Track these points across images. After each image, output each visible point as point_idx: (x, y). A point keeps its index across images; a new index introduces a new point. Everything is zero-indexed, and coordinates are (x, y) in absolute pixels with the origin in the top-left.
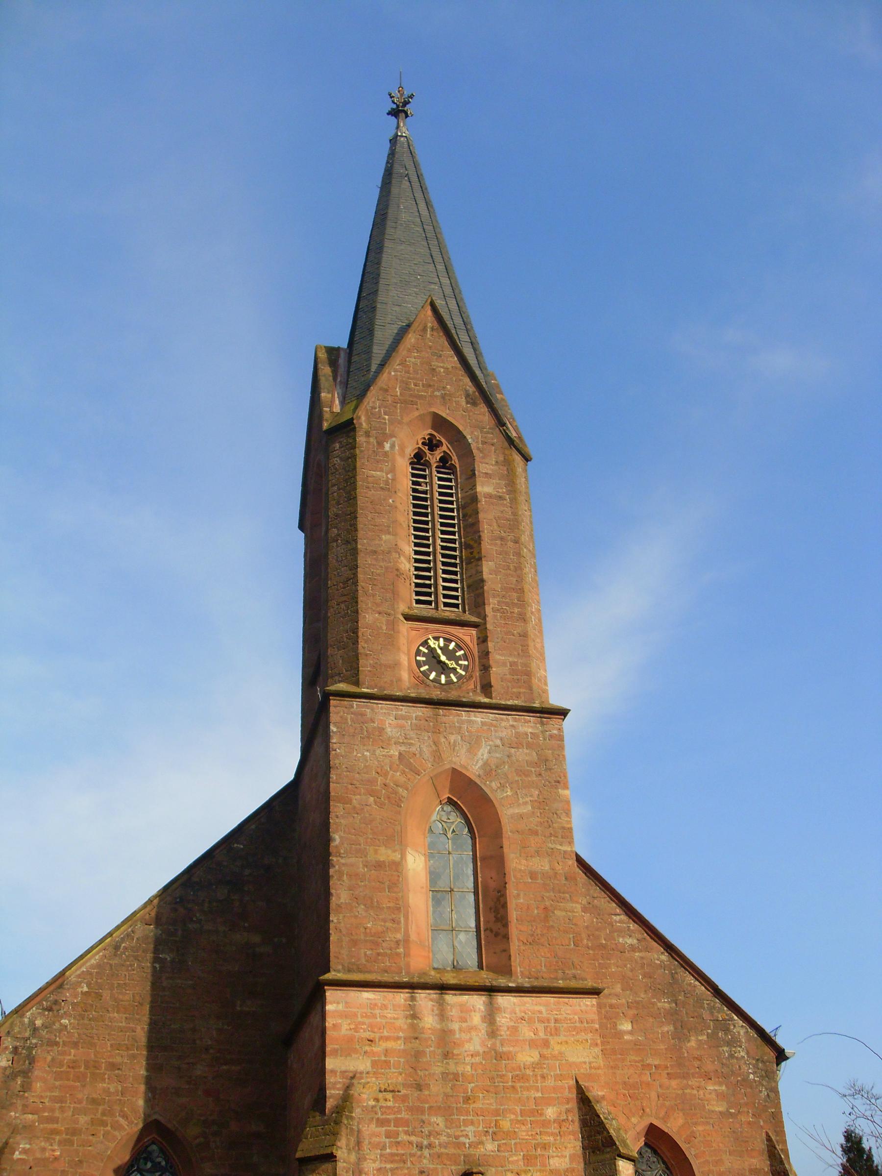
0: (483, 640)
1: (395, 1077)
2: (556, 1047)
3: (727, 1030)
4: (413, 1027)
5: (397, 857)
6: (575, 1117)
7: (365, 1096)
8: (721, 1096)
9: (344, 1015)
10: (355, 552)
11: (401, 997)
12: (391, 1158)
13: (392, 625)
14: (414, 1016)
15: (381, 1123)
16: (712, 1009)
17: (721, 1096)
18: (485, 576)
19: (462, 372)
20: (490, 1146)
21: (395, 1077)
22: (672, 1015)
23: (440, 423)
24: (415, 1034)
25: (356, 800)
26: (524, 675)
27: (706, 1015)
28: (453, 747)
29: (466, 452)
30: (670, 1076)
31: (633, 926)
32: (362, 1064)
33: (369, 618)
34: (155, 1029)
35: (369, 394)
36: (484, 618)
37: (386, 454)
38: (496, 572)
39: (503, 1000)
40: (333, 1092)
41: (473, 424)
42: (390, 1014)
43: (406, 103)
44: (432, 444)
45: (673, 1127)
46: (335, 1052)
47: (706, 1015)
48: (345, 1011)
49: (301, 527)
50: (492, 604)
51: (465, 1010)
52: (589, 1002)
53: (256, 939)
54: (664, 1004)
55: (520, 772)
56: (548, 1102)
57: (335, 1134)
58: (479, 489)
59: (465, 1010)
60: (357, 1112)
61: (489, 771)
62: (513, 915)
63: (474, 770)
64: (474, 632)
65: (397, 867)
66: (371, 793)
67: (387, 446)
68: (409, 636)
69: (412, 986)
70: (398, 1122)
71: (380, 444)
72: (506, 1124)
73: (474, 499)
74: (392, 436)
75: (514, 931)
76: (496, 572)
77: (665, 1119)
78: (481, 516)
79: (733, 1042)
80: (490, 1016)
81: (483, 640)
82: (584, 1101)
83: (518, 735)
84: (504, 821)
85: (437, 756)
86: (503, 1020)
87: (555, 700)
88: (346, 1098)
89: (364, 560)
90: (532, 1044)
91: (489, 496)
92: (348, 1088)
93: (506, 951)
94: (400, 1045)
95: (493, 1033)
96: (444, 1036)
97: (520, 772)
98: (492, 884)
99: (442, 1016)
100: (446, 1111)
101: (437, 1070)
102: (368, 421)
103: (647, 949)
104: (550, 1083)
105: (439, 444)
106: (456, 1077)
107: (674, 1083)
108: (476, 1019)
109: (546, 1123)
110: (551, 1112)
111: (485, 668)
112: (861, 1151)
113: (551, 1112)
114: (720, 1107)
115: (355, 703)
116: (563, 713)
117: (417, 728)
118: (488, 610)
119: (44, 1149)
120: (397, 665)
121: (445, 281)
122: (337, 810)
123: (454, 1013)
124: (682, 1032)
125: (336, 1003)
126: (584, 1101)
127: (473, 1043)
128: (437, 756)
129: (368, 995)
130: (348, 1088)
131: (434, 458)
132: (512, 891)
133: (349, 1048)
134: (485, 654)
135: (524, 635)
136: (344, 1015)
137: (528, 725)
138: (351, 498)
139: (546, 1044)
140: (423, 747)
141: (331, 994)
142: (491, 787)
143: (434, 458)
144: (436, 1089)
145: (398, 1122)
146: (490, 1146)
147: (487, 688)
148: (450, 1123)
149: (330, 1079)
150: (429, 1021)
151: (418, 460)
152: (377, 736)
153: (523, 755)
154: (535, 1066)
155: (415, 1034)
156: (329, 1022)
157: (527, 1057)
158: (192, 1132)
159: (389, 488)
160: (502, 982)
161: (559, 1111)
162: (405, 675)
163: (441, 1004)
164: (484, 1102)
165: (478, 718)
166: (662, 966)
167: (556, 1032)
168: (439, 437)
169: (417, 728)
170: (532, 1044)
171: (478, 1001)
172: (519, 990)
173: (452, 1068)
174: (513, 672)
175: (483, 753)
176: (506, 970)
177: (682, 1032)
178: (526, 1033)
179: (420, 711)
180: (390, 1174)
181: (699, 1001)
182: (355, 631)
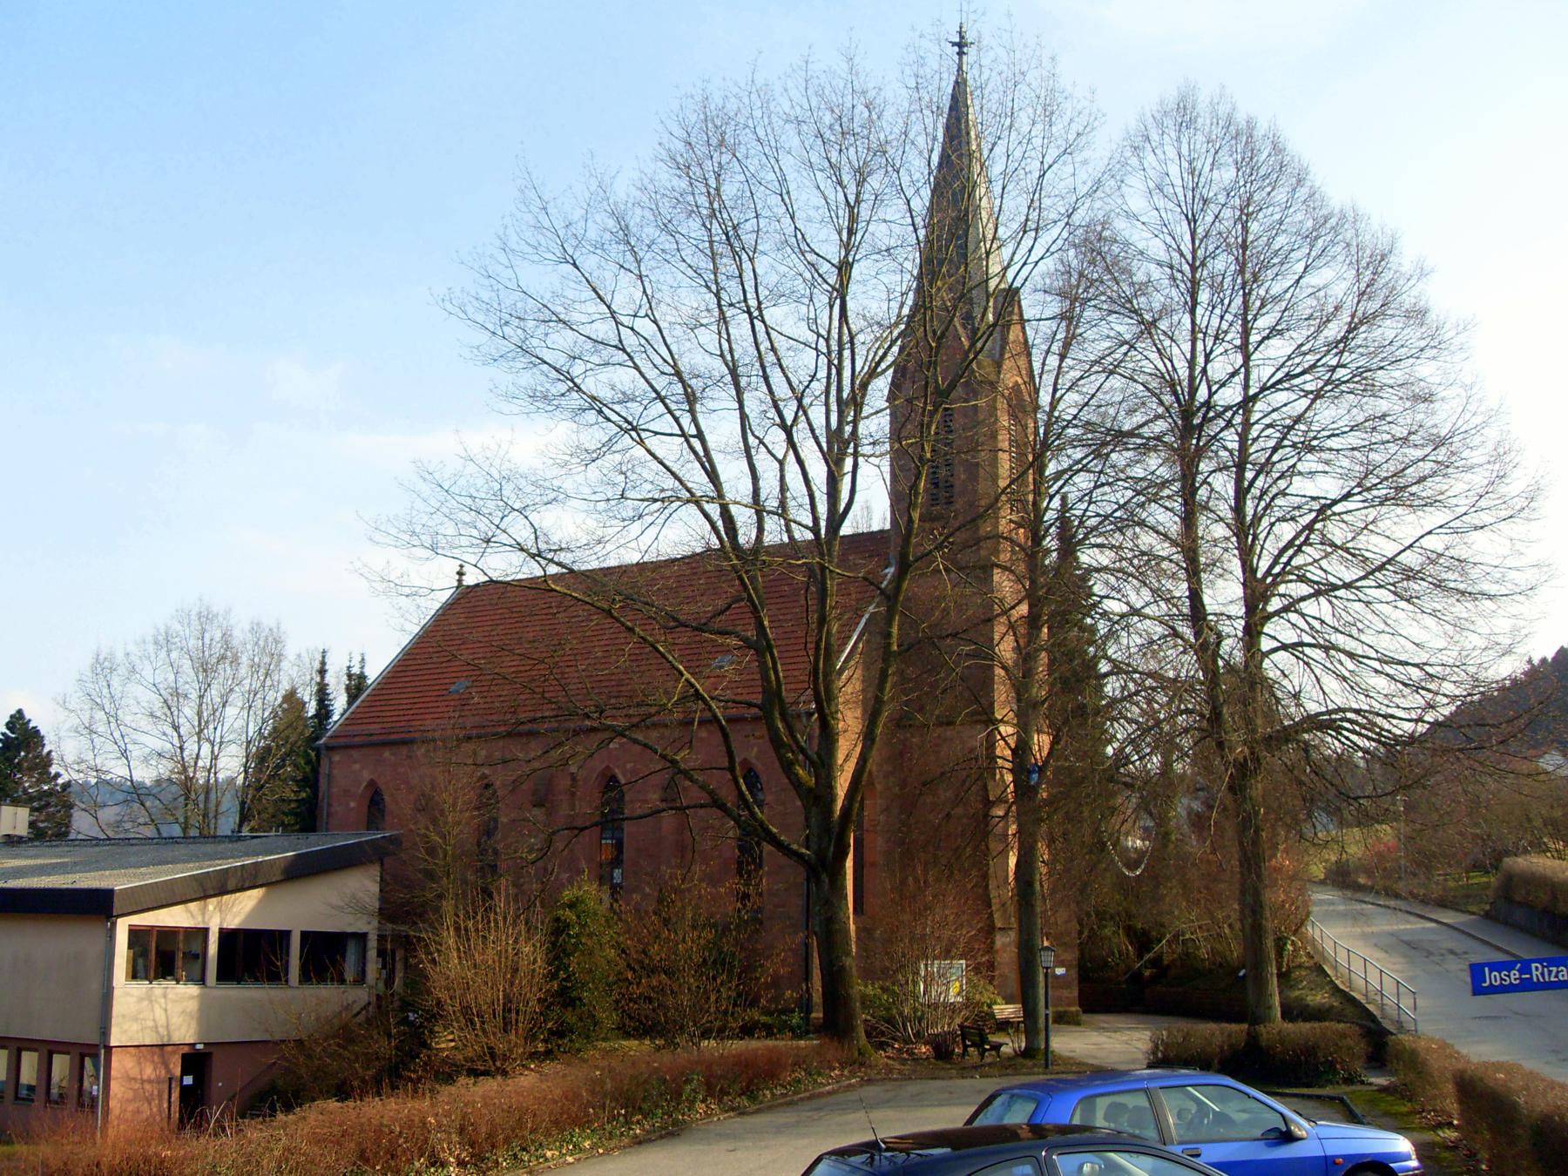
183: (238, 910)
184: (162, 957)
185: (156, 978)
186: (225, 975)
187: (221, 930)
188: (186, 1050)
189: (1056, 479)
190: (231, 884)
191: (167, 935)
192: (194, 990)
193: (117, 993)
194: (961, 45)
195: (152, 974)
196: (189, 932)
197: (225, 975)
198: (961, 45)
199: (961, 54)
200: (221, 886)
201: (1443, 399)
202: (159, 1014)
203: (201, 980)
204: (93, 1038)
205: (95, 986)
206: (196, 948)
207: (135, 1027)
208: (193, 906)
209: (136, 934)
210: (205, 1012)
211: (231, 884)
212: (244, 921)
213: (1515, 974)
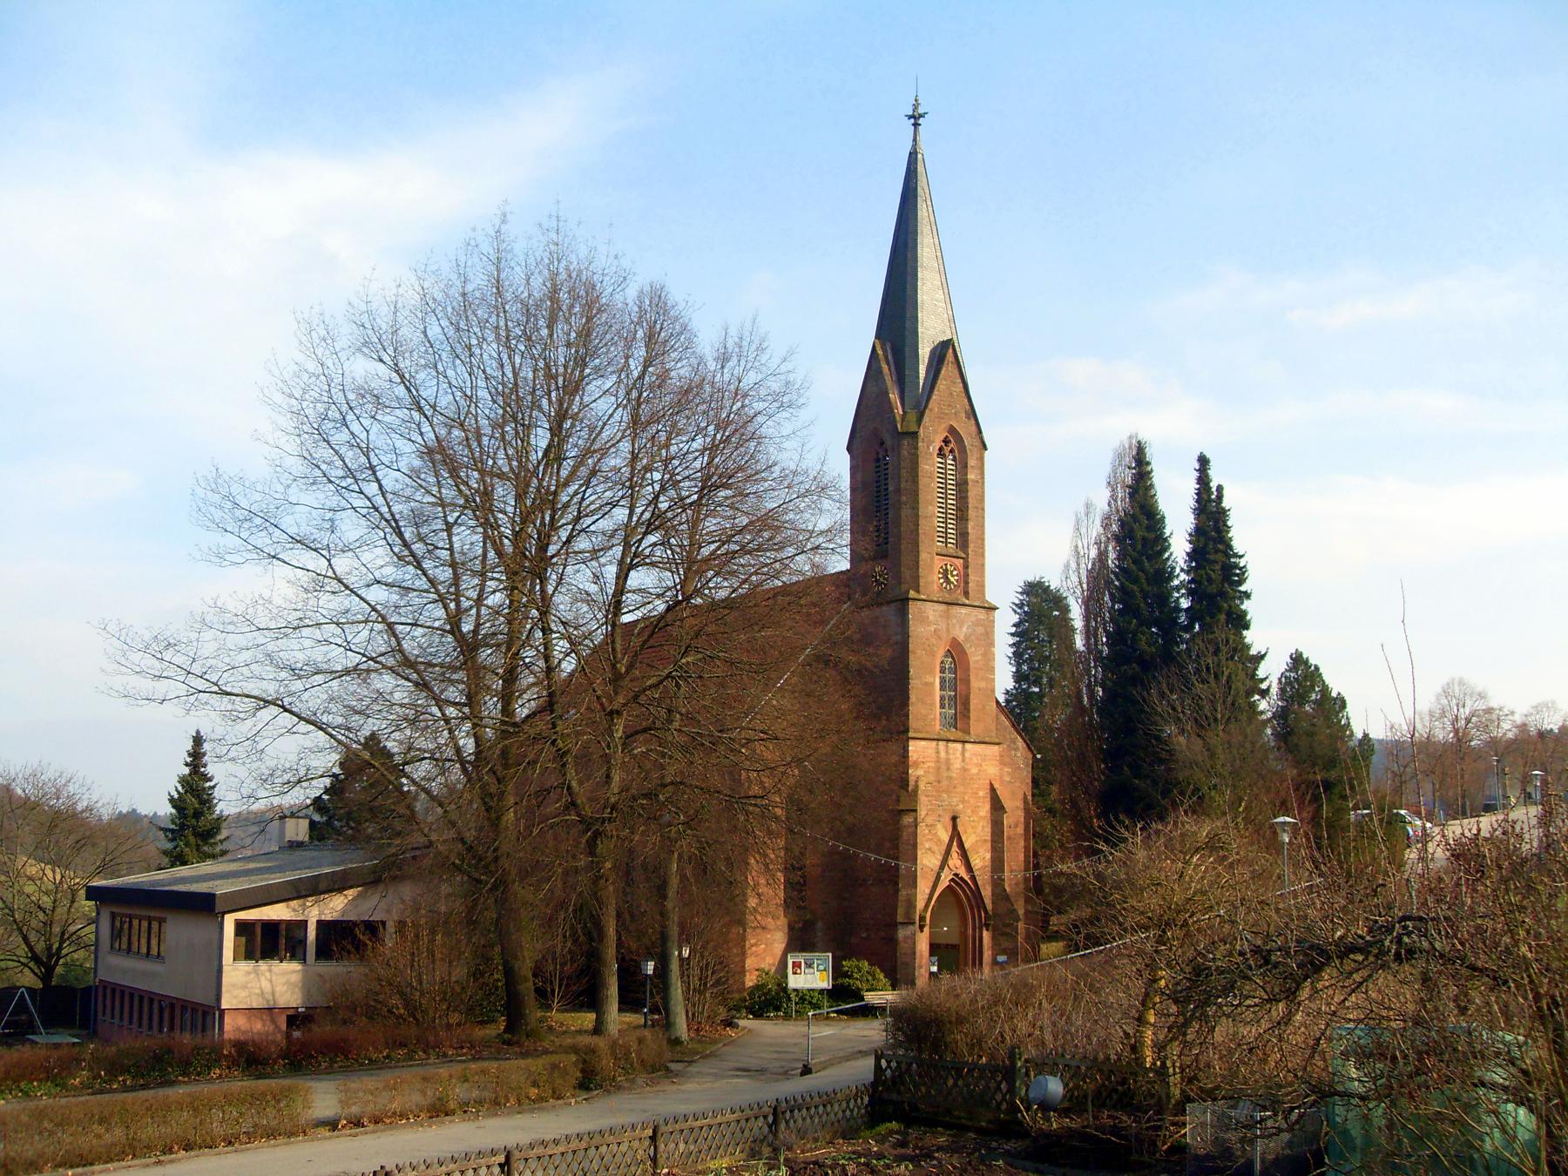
0: (966, 567)
1: (932, 778)
7: (922, 786)
21: (932, 778)
23: (952, 430)
24: (938, 761)
29: (963, 450)
40: (912, 783)
41: (965, 430)
49: (849, 449)
63: (961, 638)
68: (939, 562)
73: (966, 482)
75: (973, 715)
80: (964, 750)
81: (966, 567)
82: (993, 789)
87: (994, 603)
88: (917, 786)
96: (948, 760)
100: (947, 792)
108: (958, 754)
110: (981, 794)
111: (966, 583)
113: (981, 794)
119: (99, 1136)
126: (993, 789)
127: (957, 765)
134: (967, 575)
137: (982, 614)
141: (911, 743)
142: (966, 646)
144: (945, 783)
147: (966, 594)
150: (943, 754)
151: (941, 453)
157: (974, 771)
161: (984, 793)
164: (960, 789)
165: (964, 610)
171: (959, 746)
179: (943, 607)
180: (539, 1174)
183: (335, 906)
184: (267, 942)
185: (263, 958)
186: (323, 952)
187: (318, 922)
188: (291, 1012)
189: (593, 513)
190: (322, 886)
191: (271, 927)
192: (295, 966)
193: (225, 969)
194: (916, 118)
195: (258, 954)
196: (290, 924)
197: (323, 952)
198: (916, 118)
199: (916, 125)
200: (336, 884)
201: (723, 359)
202: (266, 985)
203: (304, 960)
204: (213, 1003)
205: (216, 963)
206: (300, 935)
207: (243, 994)
208: (294, 903)
209: (242, 928)
210: (307, 987)
211: (322, 886)
212: (344, 912)
213: (118, 1133)
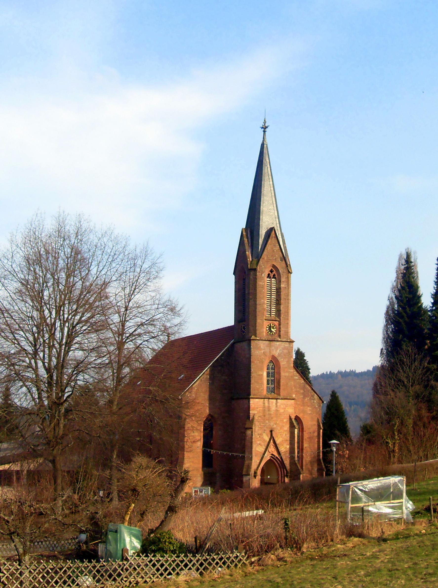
0: (280, 325)
2: (287, 409)
3: (313, 397)
4: (264, 405)
5: (262, 373)
6: (289, 421)
7: (256, 417)
8: (310, 410)
9: (253, 404)
10: (256, 304)
11: (263, 400)
12: (260, 428)
13: (263, 322)
14: (264, 404)
15: (259, 422)
16: (311, 392)
17: (310, 410)
18: (281, 309)
19: (280, 251)
20: (275, 426)
22: (303, 394)
23: (274, 266)
24: (264, 407)
25: (255, 362)
26: (287, 333)
27: (310, 394)
28: (273, 350)
29: (279, 274)
30: (301, 406)
31: (298, 375)
32: (256, 412)
33: (259, 321)
34: (210, 396)
35: (260, 261)
36: (280, 319)
37: (263, 277)
38: (283, 308)
39: (278, 400)
41: (280, 266)
42: (260, 403)
43: (265, 122)
44: (271, 271)
45: (300, 416)
46: (252, 410)
47: (310, 394)
48: (253, 403)
50: (282, 316)
51: (272, 402)
52: (293, 401)
53: (226, 378)
54: (302, 391)
55: (284, 355)
56: (284, 418)
57: (252, 425)
58: (281, 286)
59: (272, 402)
60: (255, 420)
61: (279, 355)
62: (281, 384)
63: (276, 355)
64: (278, 322)
65: (262, 375)
66: (258, 360)
67: (263, 275)
69: (264, 398)
70: (261, 422)
71: (262, 275)
72: (278, 423)
74: (264, 272)
75: (281, 387)
76: (283, 308)
77: (299, 414)
78: (282, 293)
79: (314, 399)
80: (277, 403)
81: (280, 325)
82: (290, 417)
83: (285, 347)
84: (281, 366)
85: (270, 352)
86: (278, 404)
88: (253, 418)
89: (258, 306)
90: (283, 408)
91: (284, 287)
92: (254, 416)
93: (280, 391)
94: (262, 409)
95: (276, 407)
96: (269, 407)
97: (284, 355)
98: (278, 378)
99: (269, 403)
100: (268, 420)
101: (267, 413)
102: (260, 268)
103: (300, 380)
104: (285, 415)
105: (273, 271)
106: (270, 414)
107: (302, 407)
108: (274, 404)
109: (284, 422)
111: (280, 331)
112: (335, 396)
113: (285, 420)
114: (309, 412)
115: (256, 341)
116: (293, 342)
117: (267, 346)
118: (281, 318)
120: (263, 332)
121: (277, 220)
122: (252, 364)
123: (270, 403)
124: (305, 397)
125: (252, 401)
127: (273, 408)
128: (270, 352)
129: (257, 400)
130: (254, 416)
131: (272, 275)
132: (281, 380)
133: (254, 409)
134: (280, 328)
135: (288, 323)
136: (253, 404)
137: (287, 345)
138: (255, 289)
139: (285, 408)
140: (267, 350)
141: (251, 400)
143: (272, 275)
145: (261, 422)
146: (275, 426)
147: (280, 336)
148: (269, 422)
149: (251, 415)
150: (266, 404)
152: (259, 348)
153: (285, 351)
154: (283, 412)
155: (264, 407)
156: (251, 405)
158: (216, 416)
159: (263, 287)
160: (279, 397)
161: (286, 420)
162: (265, 334)
163: (269, 401)
164: (274, 419)
165: (278, 343)
166: (303, 383)
167: (287, 406)
168: (273, 270)
169: (267, 346)
170: (283, 408)
171: (275, 401)
172: (282, 399)
173: (270, 413)
174: (285, 332)
175: (278, 351)
176: (279, 394)
177: (305, 397)
178: (282, 407)
179: (267, 342)
181: (309, 391)
182: (256, 324)
